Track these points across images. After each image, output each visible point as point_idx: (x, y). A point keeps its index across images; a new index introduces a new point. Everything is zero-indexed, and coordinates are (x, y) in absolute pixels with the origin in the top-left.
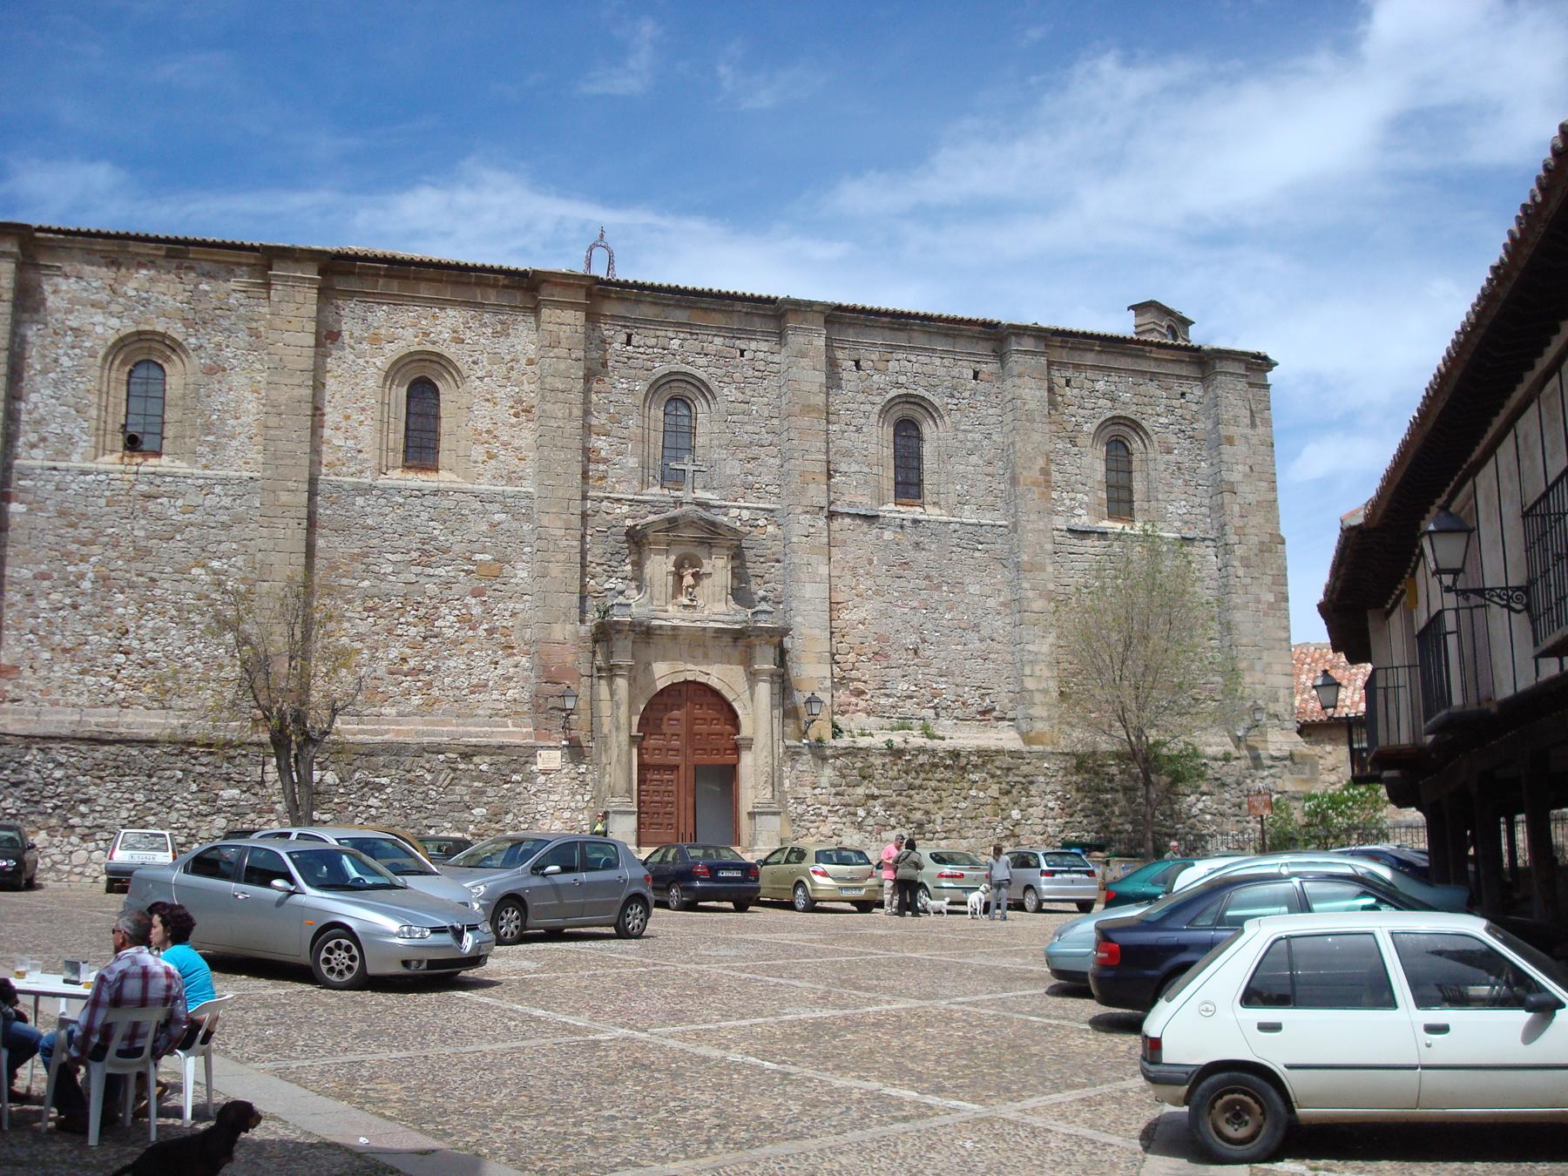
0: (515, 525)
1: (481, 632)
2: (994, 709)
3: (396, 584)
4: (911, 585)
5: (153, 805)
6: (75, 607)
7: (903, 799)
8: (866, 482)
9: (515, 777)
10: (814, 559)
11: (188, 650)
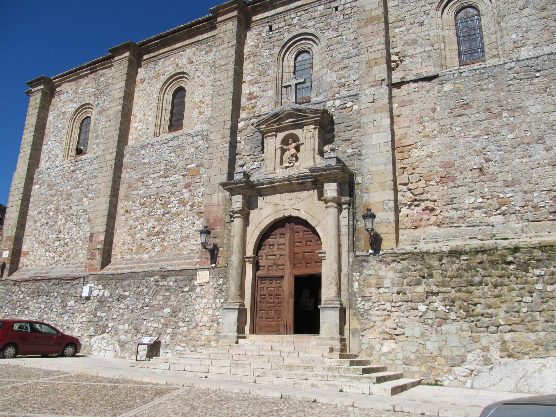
1: (188, 207)
3: (153, 190)
4: (473, 119)
6: (47, 223)
7: (464, 295)
8: (429, 57)
9: (186, 289)
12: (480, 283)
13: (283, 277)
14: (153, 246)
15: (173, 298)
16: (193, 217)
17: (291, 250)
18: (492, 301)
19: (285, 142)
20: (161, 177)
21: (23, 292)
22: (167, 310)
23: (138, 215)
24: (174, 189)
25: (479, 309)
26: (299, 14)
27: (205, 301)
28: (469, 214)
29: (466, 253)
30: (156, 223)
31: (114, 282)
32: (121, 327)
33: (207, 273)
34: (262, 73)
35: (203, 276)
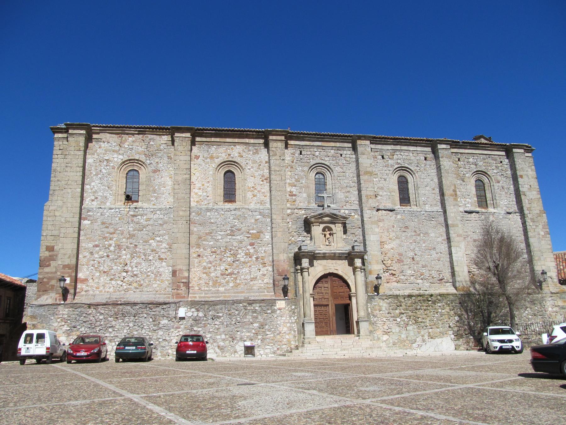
0: (264, 219)
2: (444, 279)
5: (136, 327)
8: (389, 198)
10: (373, 226)
11: (148, 270)
12: (420, 309)
13: (328, 305)
14: (228, 282)
15: (260, 317)
16: (259, 266)
17: (332, 291)
18: (424, 316)
19: (324, 230)
20: (228, 235)
21: (102, 314)
22: (256, 325)
23: (211, 260)
24: (241, 245)
25: (420, 320)
26: (319, 150)
27: (284, 318)
28: (409, 278)
29: (414, 296)
30: (228, 267)
31: (207, 307)
32: (218, 337)
33: (284, 302)
34: (297, 181)
35: (281, 304)
